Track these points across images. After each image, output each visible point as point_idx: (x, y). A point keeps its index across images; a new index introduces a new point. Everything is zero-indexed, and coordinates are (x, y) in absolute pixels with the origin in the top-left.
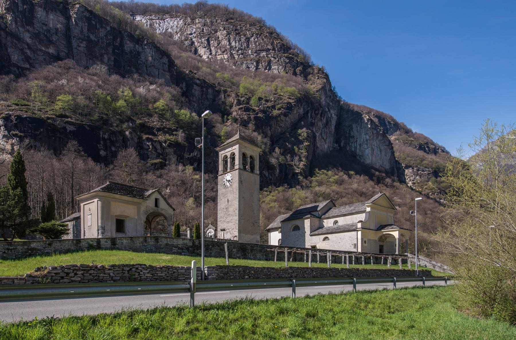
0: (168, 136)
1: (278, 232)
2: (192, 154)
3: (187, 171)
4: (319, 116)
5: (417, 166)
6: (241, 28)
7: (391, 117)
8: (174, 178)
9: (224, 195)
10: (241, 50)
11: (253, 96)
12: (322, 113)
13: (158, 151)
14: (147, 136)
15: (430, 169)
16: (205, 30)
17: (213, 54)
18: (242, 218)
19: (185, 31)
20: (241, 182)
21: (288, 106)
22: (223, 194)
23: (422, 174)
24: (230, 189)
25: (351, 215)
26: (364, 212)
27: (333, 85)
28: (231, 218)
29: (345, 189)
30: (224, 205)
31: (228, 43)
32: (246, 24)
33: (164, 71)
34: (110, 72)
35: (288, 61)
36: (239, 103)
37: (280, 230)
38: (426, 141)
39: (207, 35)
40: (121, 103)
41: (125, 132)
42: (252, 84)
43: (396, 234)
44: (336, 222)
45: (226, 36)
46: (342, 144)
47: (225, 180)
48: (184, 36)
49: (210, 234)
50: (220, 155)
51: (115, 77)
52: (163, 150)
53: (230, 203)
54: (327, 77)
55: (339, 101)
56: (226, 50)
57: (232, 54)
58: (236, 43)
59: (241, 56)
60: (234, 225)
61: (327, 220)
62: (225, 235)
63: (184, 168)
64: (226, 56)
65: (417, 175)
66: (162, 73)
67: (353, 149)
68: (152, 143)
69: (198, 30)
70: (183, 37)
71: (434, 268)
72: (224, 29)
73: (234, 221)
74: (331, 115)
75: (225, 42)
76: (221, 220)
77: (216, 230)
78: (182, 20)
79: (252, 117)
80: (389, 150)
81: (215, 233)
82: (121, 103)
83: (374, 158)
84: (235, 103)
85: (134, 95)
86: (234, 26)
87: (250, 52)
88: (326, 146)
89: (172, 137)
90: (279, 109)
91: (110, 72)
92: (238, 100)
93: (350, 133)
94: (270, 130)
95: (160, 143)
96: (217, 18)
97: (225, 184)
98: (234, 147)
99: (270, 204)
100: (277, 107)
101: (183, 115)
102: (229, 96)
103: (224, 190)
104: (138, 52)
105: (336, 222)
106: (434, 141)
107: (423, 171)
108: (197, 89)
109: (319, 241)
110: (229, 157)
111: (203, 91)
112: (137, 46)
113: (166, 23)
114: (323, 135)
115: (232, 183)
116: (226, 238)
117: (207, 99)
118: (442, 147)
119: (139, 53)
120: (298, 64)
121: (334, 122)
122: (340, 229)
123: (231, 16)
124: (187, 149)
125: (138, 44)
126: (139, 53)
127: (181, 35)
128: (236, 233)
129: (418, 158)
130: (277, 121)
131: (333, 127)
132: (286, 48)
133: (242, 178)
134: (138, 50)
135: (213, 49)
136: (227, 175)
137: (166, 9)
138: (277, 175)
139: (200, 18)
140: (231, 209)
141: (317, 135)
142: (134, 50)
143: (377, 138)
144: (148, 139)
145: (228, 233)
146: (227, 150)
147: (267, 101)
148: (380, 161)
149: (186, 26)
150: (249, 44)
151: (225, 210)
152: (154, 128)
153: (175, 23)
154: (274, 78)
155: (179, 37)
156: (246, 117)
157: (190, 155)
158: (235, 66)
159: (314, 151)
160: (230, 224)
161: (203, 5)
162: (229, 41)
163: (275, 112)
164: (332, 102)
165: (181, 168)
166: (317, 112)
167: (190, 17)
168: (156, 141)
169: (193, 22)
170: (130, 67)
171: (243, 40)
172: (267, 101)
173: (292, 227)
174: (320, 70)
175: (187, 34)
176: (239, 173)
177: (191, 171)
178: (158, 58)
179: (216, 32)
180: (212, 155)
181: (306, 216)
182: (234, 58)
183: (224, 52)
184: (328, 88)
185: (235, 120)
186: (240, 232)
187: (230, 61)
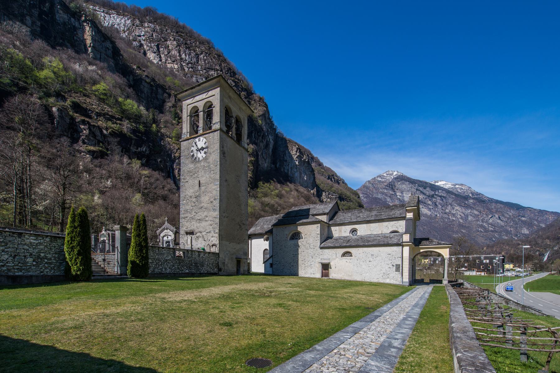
0: (110, 124)
1: (263, 239)
2: (139, 149)
3: (133, 165)
4: (261, 138)
5: (328, 191)
6: (191, 43)
8: (118, 170)
9: (192, 173)
10: (191, 64)
12: (263, 136)
13: (97, 138)
14: (83, 118)
15: (337, 195)
16: (154, 36)
17: (163, 61)
18: (224, 215)
19: (133, 31)
22: (189, 172)
24: (202, 164)
25: (379, 222)
26: (404, 218)
27: (271, 115)
28: (205, 214)
29: (285, 202)
30: (192, 191)
31: (178, 54)
32: (196, 41)
33: (108, 56)
34: (34, 35)
35: (234, 84)
37: (266, 237)
39: (156, 41)
40: (44, 74)
41: (52, 107)
43: (445, 253)
44: (354, 231)
45: (176, 47)
46: (278, 166)
47: (194, 149)
48: (132, 36)
49: (165, 238)
50: (184, 107)
51: (39, 44)
52: (105, 138)
54: (266, 106)
55: (275, 129)
56: (176, 60)
57: (182, 66)
58: (186, 56)
59: (190, 69)
60: (211, 225)
61: (340, 227)
62: (193, 241)
63: (129, 161)
64: (176, 66)
65: (329, 198)
66: (105, 58)
67: (286, 171)
68: (89, 127)
69: (148, 34)
70: (131, 37)
71: (508, 304)
72: (174, 40)
73: (211, 219)
74: (269, 139)
75: (174, 52)
76: (186, 215)
77: (177, 233)
78: (130, 20)
81: (175, 237)
82: (44, 74)
83: (301, 180)
85: (66, 69)
86: (184, 39)
87: (199, 67)
88: (266, 165)
89: (115, 125)
91: (34, 35)
93: (283, 157)
95: (100, 129)
96: (167, 28)
97: (193, 155)
98: (211, 93)
101: (129, 105)
103: (191, 166)
104: (74, 27)
105: (354, 231)
108: (146, 86)
109: (334, 257)
110: (201, 109)
111: (153, 90)
112: (73, 19)
113: (112, 18)
114: (264, 155)
115: (208, 154)
116: (195, 247)
117: (157, 98)
118: (342, 179)
119: (75, 29)
120: (243, 89)
121: (271, 146)
122: (369, 241)
123: (181, 30)
124: (133, 142)
125: (74, 18)
126: (75, 29)
127: (128, 34)
128: (215, 240)
131: (271, 150)
132: (233, 73)
133: (225, 149)
134: (74, 24)
135: (162, 56)
136: (197, 140)
137: (112, 5)
139: (150, 23)
140: (205, 199)
141: (260, 154)
142: (68, 23)
143: (304, 164)
144: (83, 122)
145: (200, 239)
146: (198, 98)
148: (305, 184)
149: (134, 27)
150: (198, 60)
151: (194, 200)
152: (93, 112)
153: (123, 21)
155: (127, 36)
157: (137, 149)
158: (185, 77)
159: (257, 168)
160: (204, 224)
161: (153, 12)
162: (179, 52)
164: (270, 128)
165: (125, 160)
166: (259, 134)
167: (139, 19)
168: (94, 126)
169: (142, 25)
170: (64, 41)
171: (193, 54)
173: (290, 235)
174: (260, 99)
175: (135, 35)
176: (221, 138)
177: (138, 166)
178: (99, 40)
179: (166, 41)
180: (162, 153)
181: (301, 222)
182: (184, 70)
183: (174, 62)
184: (267, 116)
186: (221, 238)
187: (180, 71)
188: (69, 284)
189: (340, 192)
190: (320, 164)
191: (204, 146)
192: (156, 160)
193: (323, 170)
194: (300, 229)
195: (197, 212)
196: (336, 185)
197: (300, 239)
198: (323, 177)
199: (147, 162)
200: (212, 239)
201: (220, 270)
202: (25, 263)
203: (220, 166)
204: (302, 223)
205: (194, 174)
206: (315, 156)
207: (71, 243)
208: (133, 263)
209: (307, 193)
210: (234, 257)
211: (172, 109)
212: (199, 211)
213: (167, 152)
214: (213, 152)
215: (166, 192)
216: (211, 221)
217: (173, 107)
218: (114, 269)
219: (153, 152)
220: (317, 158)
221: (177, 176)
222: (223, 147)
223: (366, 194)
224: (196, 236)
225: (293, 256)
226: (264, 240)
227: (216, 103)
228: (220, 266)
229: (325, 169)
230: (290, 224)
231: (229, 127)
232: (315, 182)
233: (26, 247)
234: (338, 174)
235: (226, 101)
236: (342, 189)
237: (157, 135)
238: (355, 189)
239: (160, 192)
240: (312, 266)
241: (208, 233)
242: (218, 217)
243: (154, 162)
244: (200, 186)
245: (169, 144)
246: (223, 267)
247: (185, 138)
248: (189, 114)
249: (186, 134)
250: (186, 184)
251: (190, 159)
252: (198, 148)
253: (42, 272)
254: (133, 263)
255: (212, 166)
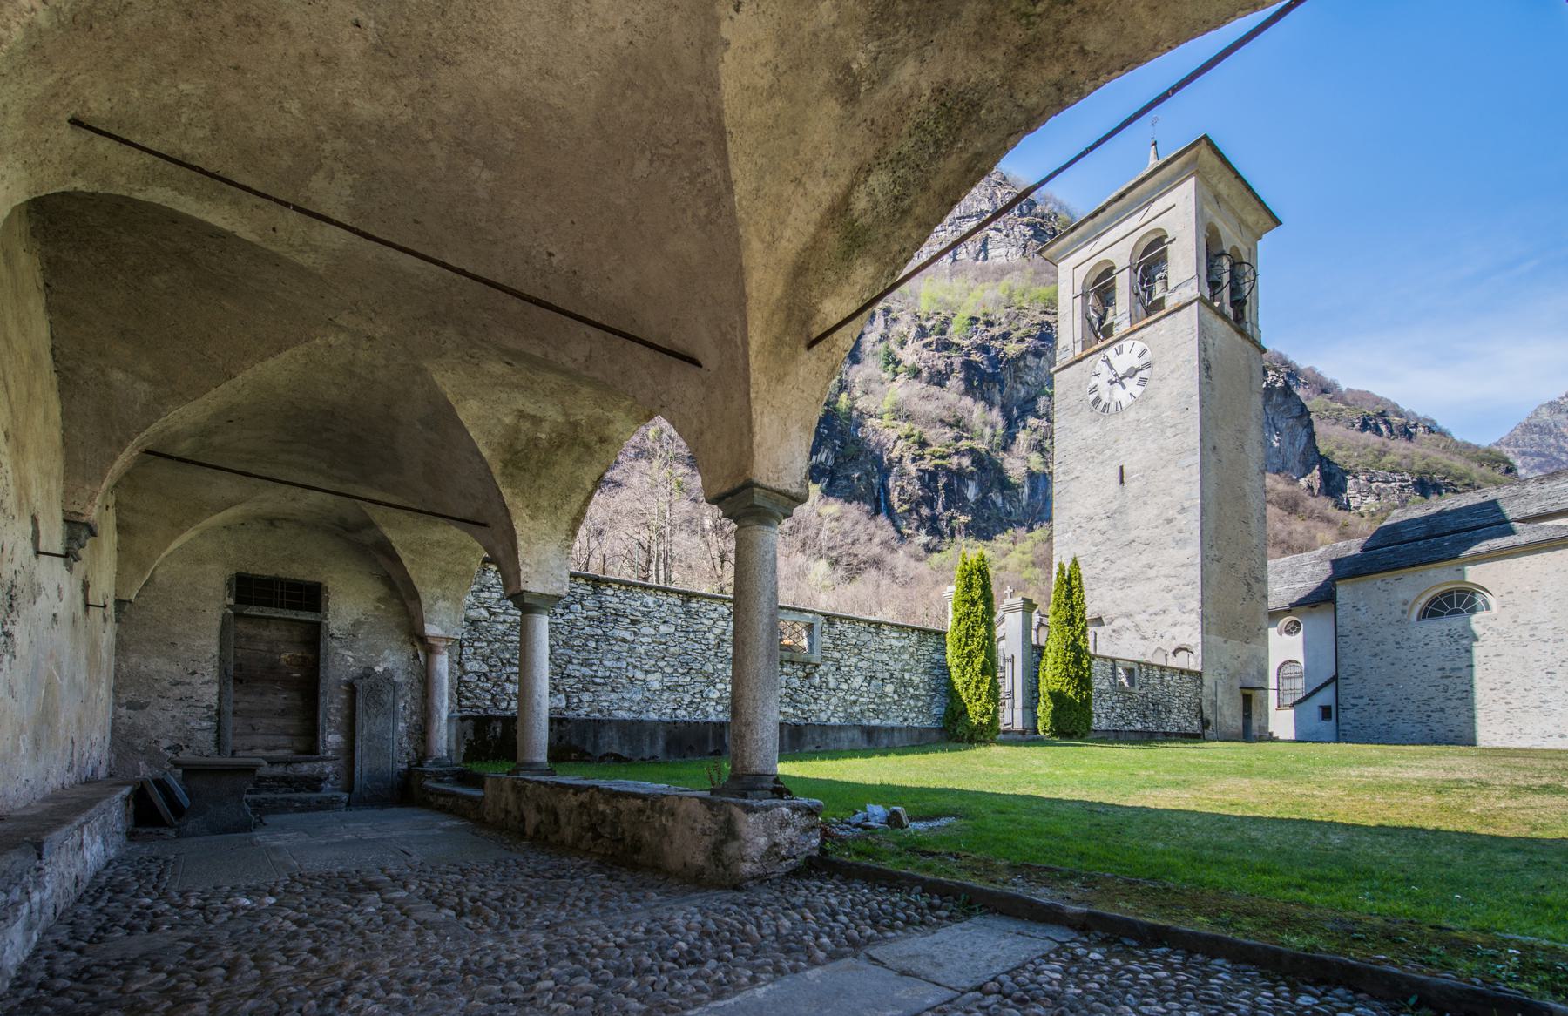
5: (1366, 471)
7: (1281, 356)
11: (954, 315)
15: (1407, 476)
20: (1208, 368)
21: (1043, 333)
23: (1384, 489)
24: (1132, 415)
35: (1031, 232)
36: (922, 333)
38: (1380, 408)
42: (950, 291)
53: (1133, 486)
65: (1370, 492)
79: (957, 361)
80: (1300, 429)
84: (913, 334)
90: (1021, 340)
92: (920, 326)
94: (1001, 391)
97: (1098, 399)
99: (1021, 572)
100: (1016, 335)
102: (895, 320)
103: (1091, 431)
106: (1401, 406)
107: (1387, 482)
115: (1149, 385)
129: (1368, 449)
130: (1017, 369)
136: (1110, 353)
138: (1024, 502)
140: (1142, 518)
147: (990, 324)
151: (1103, 525)
154: (1002, 272)
156: (941, 365)
160: (1139, 589)
163: (1012, 349)
172: (990, 324)
173: (1423, 601)
180: (862, 458)
181: (1481, 547)
185: (916, 373)
188: (943, 751)
189: (1419, 465)
190: (1325, 389)
191: (1137, 364)
192: (848, 477)
193: (1340, 405)
194: (1473, 574)
195: (1113, 558)
196: (1399, 446)
197: (1473, 610)
198: (1340, 428)
199: (830, 484)
200: (1175, 631)
201: (1205, 724)
202: (883, 696)
203: (1201, 407)
204: (1490, 551)
205: (1101, 452)
206: (1302, 362)
207: (966, 644)
208: (1057, 697)
209: (1289, 488)
210: (1237, 684)
211: (881, 347)
212: (1120, 554)
213: (872, 452)
214: (1172, 372)
215: (878, 550)
216: (1167, 577)
217: (881, 341)
218: (1012, 716)
219: (841, 460)
220: (1312, 370)
221: (896, 507)
222: (1205, 349)
223: (1539, 454)
224: (1111, 627)
225: (1440, 674)
226: (1280, 634)
227: (1178, 228)
228: (1205, 711)
229: (1349, 398)
230: (1421, 563)
231: (1214, 285)
232: (1316, 449)
233: (885, 657)
234: (1405, 406)
235: (1208, 210)
236: (1428, 452)
237: (849, 418)
238: (1484, 440)
239: (863, 551)
240: (1553, 706)
241: (1156, 614)
242: (1198, 560)
243: (845, 482)
244: (1122, 482)
245: (875, 431)
246: (1212, 718)
247: (1070, 358)
248: (1079, 291)
249: (1071, 347)
250: (1075, 483)
251: (1086, 414)
252: (1116, 375)
253: (906, 720)
254: (1057, 697)
255: (1169, 413)
